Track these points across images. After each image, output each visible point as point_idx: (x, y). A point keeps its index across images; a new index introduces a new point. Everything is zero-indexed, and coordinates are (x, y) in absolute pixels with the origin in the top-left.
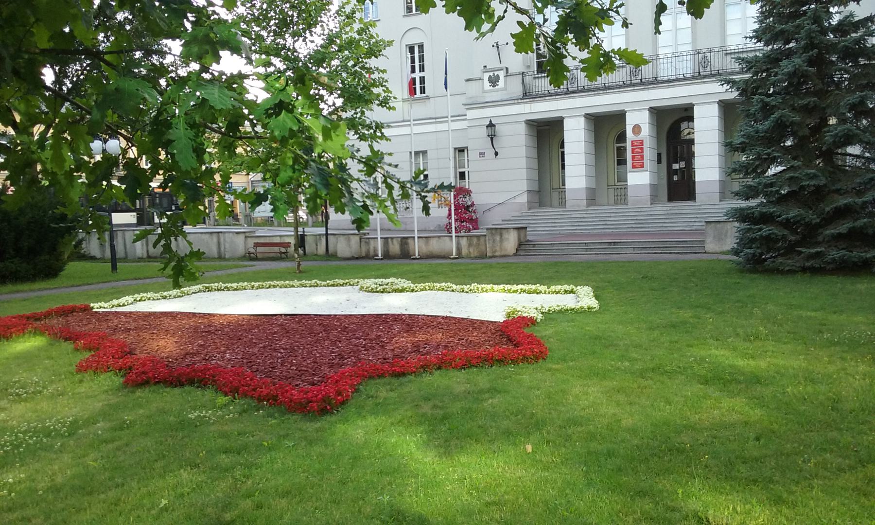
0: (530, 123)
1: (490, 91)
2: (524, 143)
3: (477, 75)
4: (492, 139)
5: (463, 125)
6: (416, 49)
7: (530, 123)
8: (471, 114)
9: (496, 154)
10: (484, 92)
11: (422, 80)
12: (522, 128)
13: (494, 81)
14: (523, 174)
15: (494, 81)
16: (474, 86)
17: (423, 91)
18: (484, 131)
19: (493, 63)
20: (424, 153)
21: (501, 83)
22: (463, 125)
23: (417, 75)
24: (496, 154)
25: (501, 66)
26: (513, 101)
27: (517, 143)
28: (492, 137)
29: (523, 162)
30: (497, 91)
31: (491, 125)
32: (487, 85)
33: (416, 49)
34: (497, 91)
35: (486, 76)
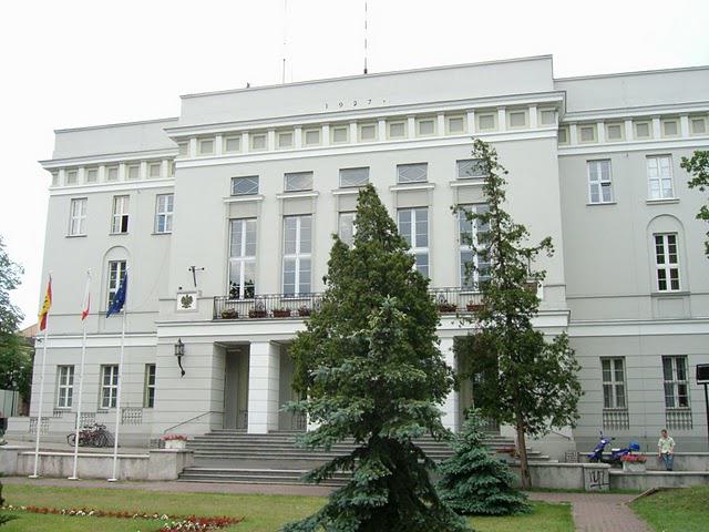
0: (218, 346)
1: (179, 312)
2: (267, 364)
3: (172, 295)
4: (179, 358)
5: (154, 342)
6: (665, 239)
7: (218, 346)
8: (162, 332)
9: (183, 373)
10: (177, 312)
11: (674, 273)
12: (211, 350)
13: (187, 302)
14: (208, 395)
15: (187, 302)
16: (169, 307)
17: (675, 285)
18: (172, 350)
19: (188, 286)
20: (619, 361)
21: (193, 305)
22: (154, 342)
23: (667, 266)
24: (183, 373)
25: (195, 289)
26: (203, 323)
27: (205, 365)
28: (180, 356)
29: (208, 384)
30: (189, 312)
31: (181, 345)
32: (180, 305)
33: (665, 239)
34: (189, 312)
35: (180, 297)
